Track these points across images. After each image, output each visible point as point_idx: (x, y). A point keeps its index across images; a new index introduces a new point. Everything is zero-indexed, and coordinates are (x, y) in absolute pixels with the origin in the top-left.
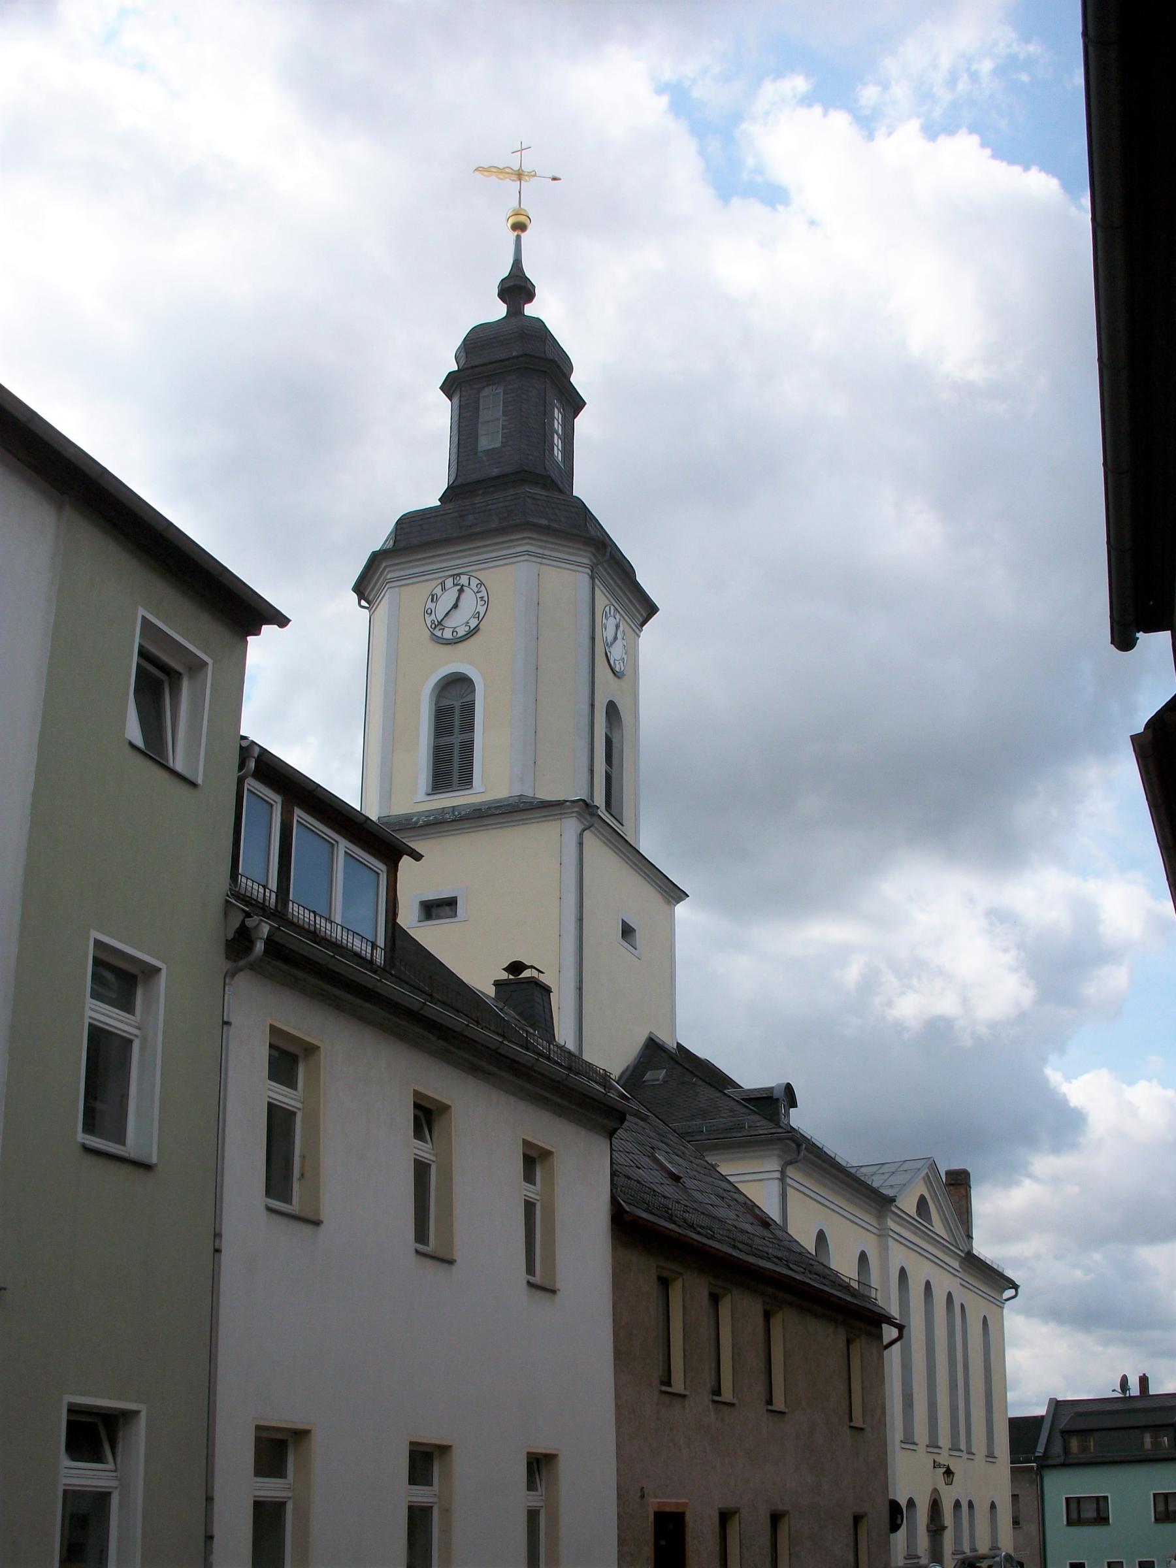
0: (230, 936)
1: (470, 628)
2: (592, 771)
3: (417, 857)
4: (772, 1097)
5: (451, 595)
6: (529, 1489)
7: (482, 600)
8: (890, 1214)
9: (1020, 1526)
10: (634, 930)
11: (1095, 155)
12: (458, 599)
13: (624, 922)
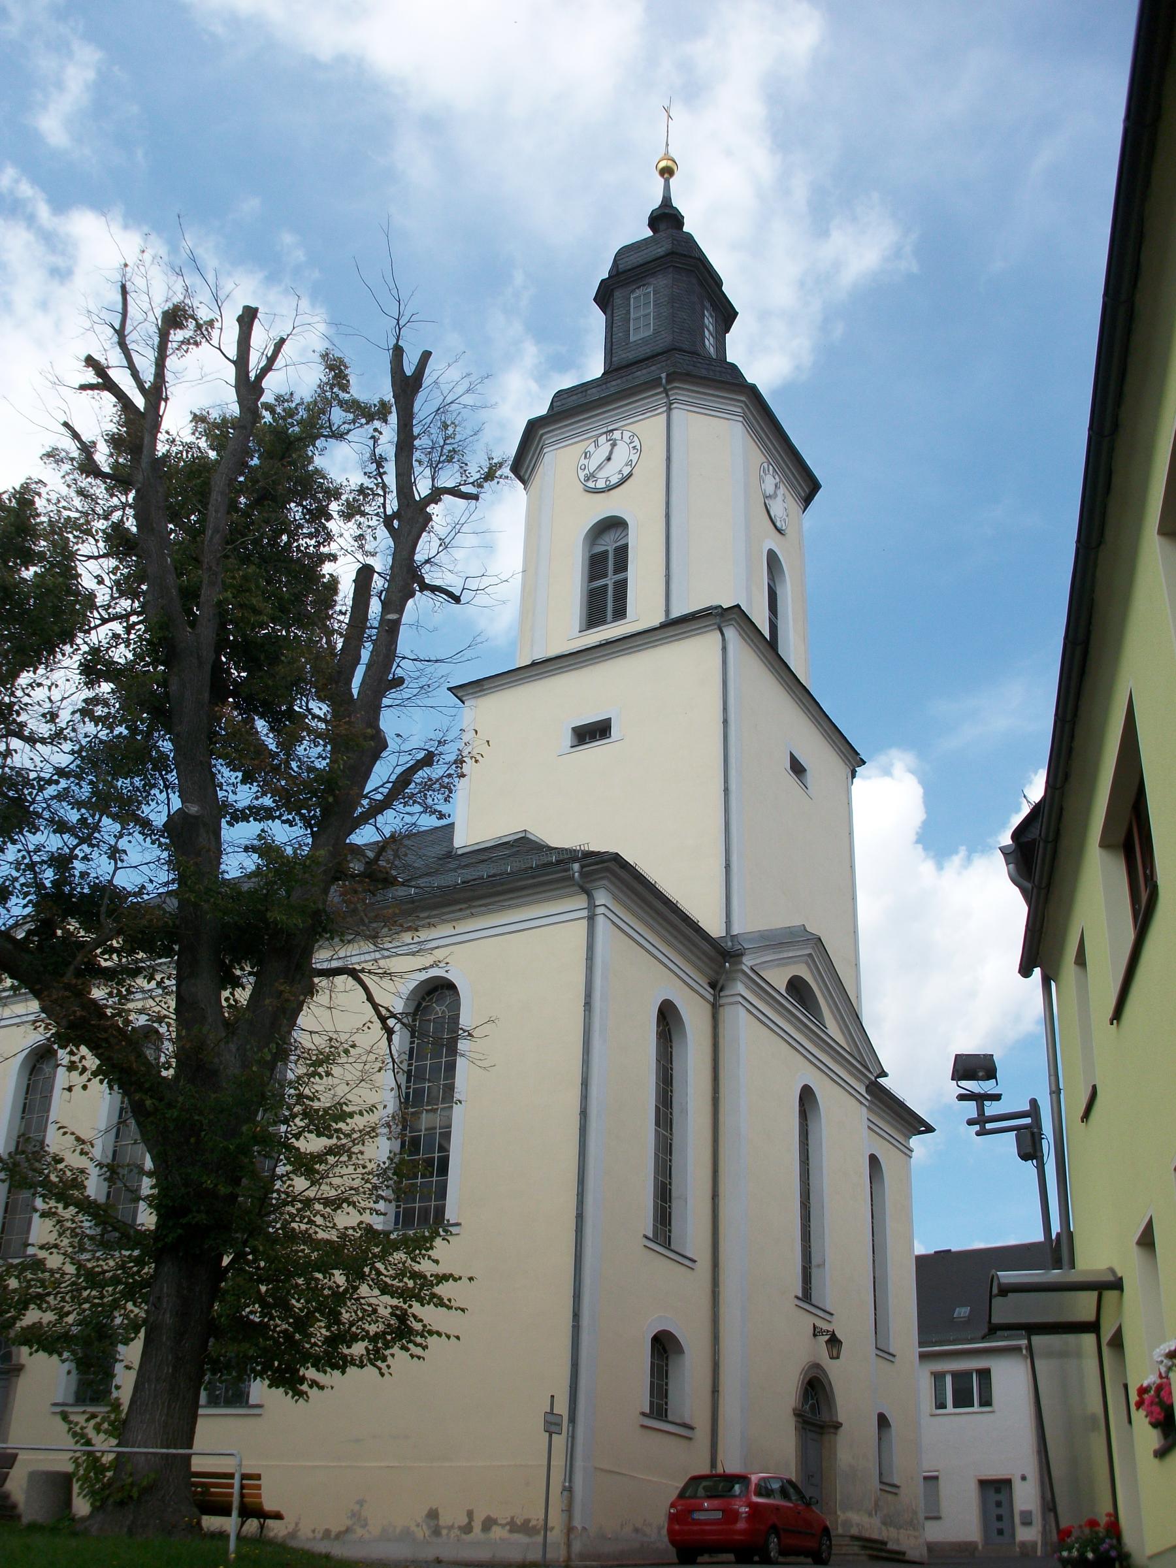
3: (643, 1414)
5: (605, 449)
6: (430, 353)
10: (805, 770)
11: (1063, 684)
12: (611, 452)
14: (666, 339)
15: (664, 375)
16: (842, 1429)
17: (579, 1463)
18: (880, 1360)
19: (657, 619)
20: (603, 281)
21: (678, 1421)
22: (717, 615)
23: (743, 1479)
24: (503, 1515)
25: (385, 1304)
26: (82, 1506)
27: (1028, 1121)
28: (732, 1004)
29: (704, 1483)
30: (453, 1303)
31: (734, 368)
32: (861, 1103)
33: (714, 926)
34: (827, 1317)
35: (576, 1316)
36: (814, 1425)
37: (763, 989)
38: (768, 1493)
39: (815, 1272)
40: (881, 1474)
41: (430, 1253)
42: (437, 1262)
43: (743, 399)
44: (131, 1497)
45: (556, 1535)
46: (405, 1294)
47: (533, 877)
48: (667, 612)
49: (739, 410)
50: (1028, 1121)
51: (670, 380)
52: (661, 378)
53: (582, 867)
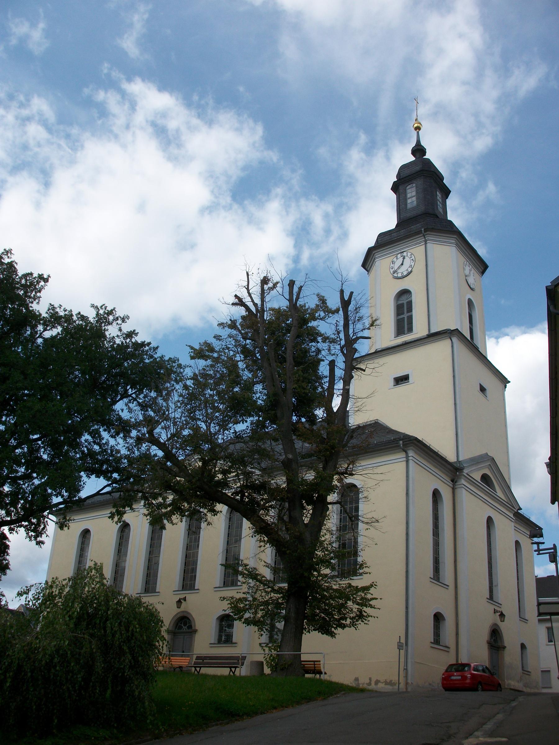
3: (431, 643)
9: (369, 499)
12: (403, 261)
13: (480, 385)
14: (422, 209)
15: (423, 229)
16: (506, 649)
17: (409, 660)
18: (521, 622)
19: (425, 333)
20: (394, 182)
21: (443, 645)
22: (449, 333)
23: (468, 665)
24: (382, 679)
25: (355, 607)
26: (267, 670)
27: (552, 551)
28: (459, 488)
29: (454, 667)
30: (375, 607)
31: (450, 222)
32: (511, 521)
33: (451, 457)
34: (499, 606)
35: (407, 608)
36: (494, 647)
37: (471, 481)
38: (477, 670)
39: (494, 588)
40: (523, 667)
41: (369, 592)
42: (372, 594)
43: (455, 237)
44: (285, 668)
45: (402, 685)
46: (362, 605)
47: (385, 446)
48: (429, 330)
49: (454, 242)
50: (552, 551)
51: (425, 231)
52: (421, 230)
53: (403, 442)
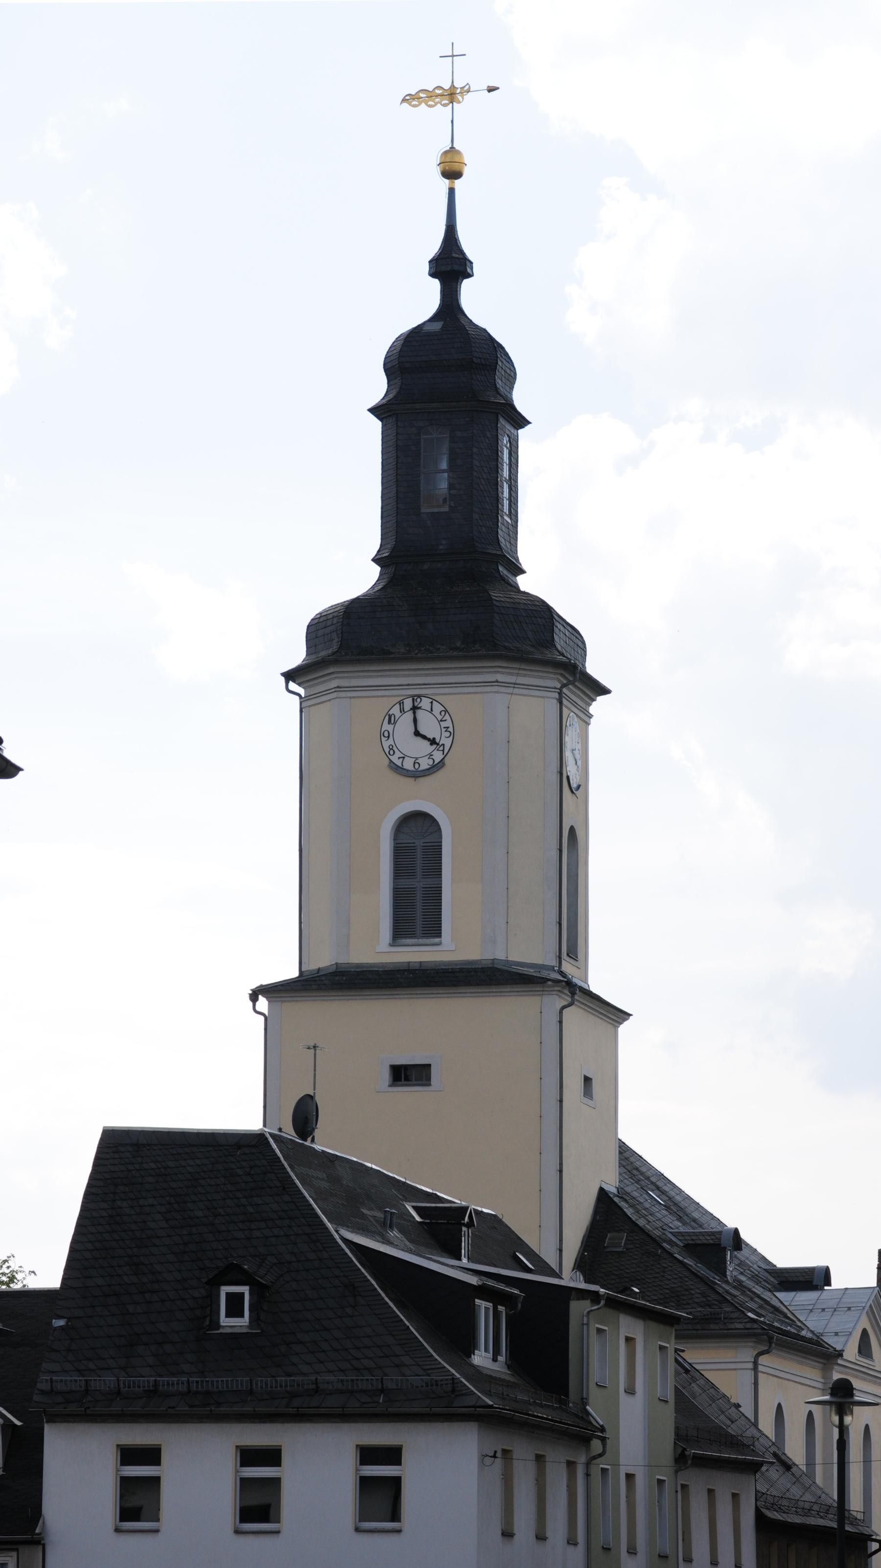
0: (677, 1456)
1: (434, 761)
2: (560, 924)
4: (720, 1244)
7: (446, 731)
8: (836, 1367)
12: (424, 737)
